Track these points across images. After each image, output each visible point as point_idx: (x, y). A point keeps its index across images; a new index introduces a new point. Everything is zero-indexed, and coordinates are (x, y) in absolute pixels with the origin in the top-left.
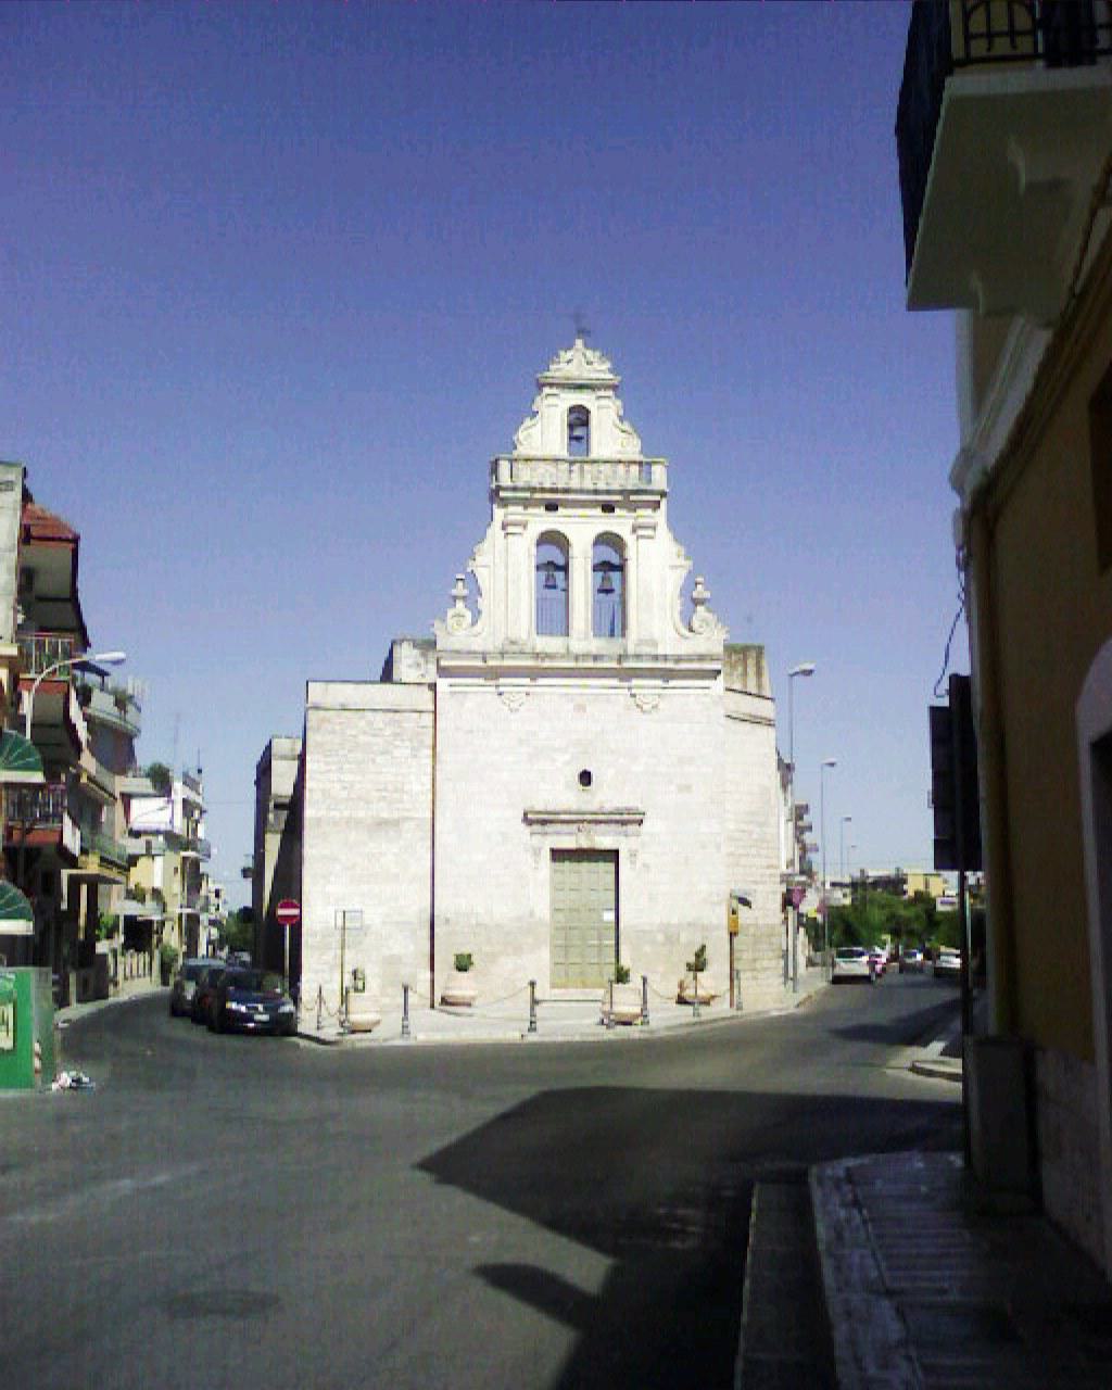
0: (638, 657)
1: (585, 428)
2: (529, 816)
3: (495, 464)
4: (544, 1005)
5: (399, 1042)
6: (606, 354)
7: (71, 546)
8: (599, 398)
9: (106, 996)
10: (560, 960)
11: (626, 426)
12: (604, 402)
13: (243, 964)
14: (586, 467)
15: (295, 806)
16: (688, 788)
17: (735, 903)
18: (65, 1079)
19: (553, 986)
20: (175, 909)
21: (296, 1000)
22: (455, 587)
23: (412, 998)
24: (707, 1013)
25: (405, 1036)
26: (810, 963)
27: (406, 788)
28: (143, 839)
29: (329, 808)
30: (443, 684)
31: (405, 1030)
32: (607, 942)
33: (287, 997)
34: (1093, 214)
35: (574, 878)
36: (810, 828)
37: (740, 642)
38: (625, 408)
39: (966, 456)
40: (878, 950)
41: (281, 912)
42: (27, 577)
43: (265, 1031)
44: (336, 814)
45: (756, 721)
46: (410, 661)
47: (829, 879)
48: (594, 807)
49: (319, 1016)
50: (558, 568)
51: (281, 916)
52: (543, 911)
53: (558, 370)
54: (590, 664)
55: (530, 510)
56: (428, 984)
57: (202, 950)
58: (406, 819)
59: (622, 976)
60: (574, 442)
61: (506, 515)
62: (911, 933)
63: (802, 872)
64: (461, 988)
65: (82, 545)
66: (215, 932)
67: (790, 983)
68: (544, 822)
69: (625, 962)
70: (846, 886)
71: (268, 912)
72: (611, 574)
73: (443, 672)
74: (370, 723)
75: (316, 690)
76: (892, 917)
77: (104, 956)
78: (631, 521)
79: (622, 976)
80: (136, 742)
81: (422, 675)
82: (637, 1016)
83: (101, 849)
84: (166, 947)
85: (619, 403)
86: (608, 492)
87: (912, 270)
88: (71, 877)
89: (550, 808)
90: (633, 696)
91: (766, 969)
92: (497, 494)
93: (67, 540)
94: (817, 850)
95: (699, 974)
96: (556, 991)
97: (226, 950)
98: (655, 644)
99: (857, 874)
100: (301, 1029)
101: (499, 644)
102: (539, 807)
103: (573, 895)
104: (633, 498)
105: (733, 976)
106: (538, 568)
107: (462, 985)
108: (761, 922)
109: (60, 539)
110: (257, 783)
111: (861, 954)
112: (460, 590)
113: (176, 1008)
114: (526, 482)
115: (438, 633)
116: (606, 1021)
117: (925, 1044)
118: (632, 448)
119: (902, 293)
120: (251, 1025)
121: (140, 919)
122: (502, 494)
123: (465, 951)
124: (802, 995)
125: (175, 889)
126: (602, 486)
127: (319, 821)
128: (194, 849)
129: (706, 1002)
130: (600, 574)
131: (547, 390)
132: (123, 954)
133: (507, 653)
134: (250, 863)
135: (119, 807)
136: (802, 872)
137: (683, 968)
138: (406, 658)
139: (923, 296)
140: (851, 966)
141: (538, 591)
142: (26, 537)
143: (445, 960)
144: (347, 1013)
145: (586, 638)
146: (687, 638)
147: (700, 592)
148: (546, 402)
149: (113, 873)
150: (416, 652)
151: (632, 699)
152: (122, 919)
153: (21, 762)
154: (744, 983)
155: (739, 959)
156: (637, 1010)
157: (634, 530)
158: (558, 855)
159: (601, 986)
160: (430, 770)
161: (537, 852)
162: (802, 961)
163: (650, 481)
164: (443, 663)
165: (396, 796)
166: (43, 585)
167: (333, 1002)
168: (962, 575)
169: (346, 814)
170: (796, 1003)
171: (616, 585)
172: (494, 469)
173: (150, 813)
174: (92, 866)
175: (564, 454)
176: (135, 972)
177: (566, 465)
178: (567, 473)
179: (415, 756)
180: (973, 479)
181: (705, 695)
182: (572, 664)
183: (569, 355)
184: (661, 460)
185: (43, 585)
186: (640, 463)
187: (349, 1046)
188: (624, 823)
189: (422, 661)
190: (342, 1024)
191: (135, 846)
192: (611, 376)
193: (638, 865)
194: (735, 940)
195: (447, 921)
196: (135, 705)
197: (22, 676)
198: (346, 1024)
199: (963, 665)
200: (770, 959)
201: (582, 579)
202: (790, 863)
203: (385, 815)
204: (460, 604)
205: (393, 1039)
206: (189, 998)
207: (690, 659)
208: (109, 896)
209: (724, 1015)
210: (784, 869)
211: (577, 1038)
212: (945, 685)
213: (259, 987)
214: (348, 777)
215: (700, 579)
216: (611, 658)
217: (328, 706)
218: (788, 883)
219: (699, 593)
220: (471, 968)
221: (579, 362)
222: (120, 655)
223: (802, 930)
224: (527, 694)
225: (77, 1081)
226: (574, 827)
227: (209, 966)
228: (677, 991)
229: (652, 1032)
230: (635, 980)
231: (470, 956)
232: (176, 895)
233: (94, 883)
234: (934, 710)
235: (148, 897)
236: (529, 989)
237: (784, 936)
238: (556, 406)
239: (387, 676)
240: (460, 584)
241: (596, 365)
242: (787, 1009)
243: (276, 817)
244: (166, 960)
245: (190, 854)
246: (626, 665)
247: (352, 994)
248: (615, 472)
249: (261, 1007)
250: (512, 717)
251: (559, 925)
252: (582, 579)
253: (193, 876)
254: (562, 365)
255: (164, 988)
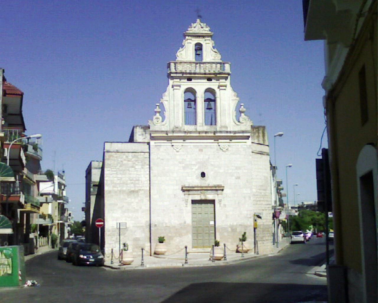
0: (221, 132)
1: (201, 51)
2: (183, 188)
3: (169, 64)
4: (190, 254)
5: (141, 268)
6: (208, 25)
7: (20, 96)
8: (205, 40)
9: (32, 253)
10: (196, 238)
11: (215, 50)
12: (207, 42)
13: (82, 241)
14: (202, 65)
15: (101, 186)
16: (238, 178)
17: (256, 218)
18: (29, 283)
19: (193, 247)
20: (56, 222)
21: (103, 253)
22: (156, 108)
23: (144, 252)
24: (246, 256)
25: (143, 266)
26: (284, 236)
27: (140, 179)
28: (44, 197)
29: (113, 187)
30: (152, 143)
31: (142, 264)
32: (211, 232)
33: (100, 253)
34: (357, 21)
35: (199, 210)
36: (283, 189)
37: (257, 125)
38: (215, 43)
39: (327, 79)
40: (308, 231)
41: (97, 223)
42: (5, 107)
43: (92, 265)
44: (116, 189)
45: (261, 153)
46: (140, 133)
47: (290, 206)
48: (206, 185)
49: (112, 259)
50: (192, 101)
51: (97, 225)
52: (189, 220)
53: (191, 30)
54: (204, 135)
55: (182, 81)
56: (149, 248)
57: (66, 235)
58: (140, 190)
59: (217, 244)
60: (197, 56)
61: (173, 82)
62: (320, 225)
63: (280, 205)
64: (161, 249)
65: (24, 96)
66: (69, 228)
67: (276, 244)
68: (189, 190)
69: (218, 239)
70: (296, 208)
71: (92, 223)
72: (211, 103)
73: (152, 138)
74: (127, 157)
75: (108, 146)
76: (312, 220)
77: (32, 239)
78: (218, 84)
79: (217, 244)
80: (41, 162)
81: (145, 138)
82: (222, 257)
83: (31, 201)
84: (53, 235)
85: (213, 42)
86: (210, 74)
87: (306, 26)
88: (21, 212)
89: (191, 185)
90: (219, 145)
91: (267, 240)
92: (170, 74)
93: (19, 95)
94: (286, 196)
95: (244, 242)
96: (194, 249)
97: (73, 235)
98: (227, 128)
99: (301, 204)
100: (106, 264)
101: (172, 128)
102: (187, 185)
103: (200, 215)
104: (218, 76)
105: (255, 243)
106: (185, 101)
107: (161, 248)
108: (265, 224)
109: (17, 95)
110: (86, 177)
111: (301, 233)
112: (157, 109)
113: (60, 257)
114: (180, 70)
115: (150, 124)
116: (211, 259)
117: (321, 266)
118: (218, 58)
119: (303, 35)
120: (88, 263)
121: (44, 225)
122: (172, 75)
123: (162, 236)
124: (280, 248)
125: (56, 214)
126: (207, 72)
127: (110, 192)
128: (62, 200)
129: (246, 252)
130: (207, 102)
131: (187, 38)
132: (39, 238)
133: (175, 131)
134: (84, 206)
135: (36, 187)
136: (280, 205)
137: (238, 240)
138: (138, 132)
139: (309, 36)
140: (298, 238)
141: (185, 108)
142: (5, 94)
143: (155, 239)
144: (122, 258)
145: (202, 126)
146: (237, 125)
147: (242, 109)
148: (187, 42)
149: (35, 210)
150: (142, 130)
151: (219, 147)
152: (38, 225)
153: (6, 174)
154: (259, 245)
155: (257, 237)
156: (222, 255)
157: (219, 88)
158: (194, 202)
159: (210, 247)
160: (148, 173)
161: (187, 201)
162: (280, 235)
163: (224, 70)
164: (152, 135)
165: (137, 182)
166: (10, 110)
167: (117, 254)
168: (326, 117)
169: (119, 189)
170: (278, 251)
171: (213, 106)
172: (169, 66)
173: (46, 187)
174: (28, 208)
175: (194, 60)
176: (43, 244)
177: (194, 64)
178: (195, 68)
179: (143, 168)
180: (329, 87)
181: (245, 145)
182: (198, 135)
183: (195, 25)
184: (228, 62)
185: (10, 110)
186: (220, 63)
187: (123, 269)
188: (217, 190)
189: (144, 133)
190: (120, 262)
191: (42, 199)
192: (209, 32)
193: (222, 205)
194: (256, 230)
195: (155, 225)
196: (40, 148)
197: (5, 143)
198: (122, 262)
199: (326, 146)
200: (268, 236)
201: (201, 105)
202: (276, 202)
203: (133, 189)
204: (158, 114)
205: (138, 267)
206: (65, 253)
207: (239, 132)
208: (33, 217)
209: (252, 256)
210: (273, 204)
211: (202, 265)
212: (320, 152)
213: (90, 250)
214: (120, 176)
215: (242, 104)
216: (211, 132)
217: (112, 151)
218: (275, 209)
219: (242, 109)
220: (164, 242)
221: (198, 27)
222: (39, 135)
223: (280, 225)
224: (182, 146)
225: (33, 284)
226: (199, 192)
227: (72, 242)
228: (236, 248)
229: (227, 263)
230: (221, 245)
231: (164, 237)
232: (56, 216)
233: (28, 213)
234: (317, 160)
235: (47, 217)
236: (185, 249)
237: (273, 228)
238: (191, 43)
239: (131, 140)
240: (157, 107)
241: (205, 28)
242: (274, 254)
243: (94, 190)
244: (54, 239)
245: (61, 201)
246: (217, 135)
247: (124, 252)
248: (212, 67)
249: (91, 257)
250: (178, 153)
251: (194, 226)
252: (201, 105)
253: (62, 210)
254: (193, 28)
255: (53, 249)
